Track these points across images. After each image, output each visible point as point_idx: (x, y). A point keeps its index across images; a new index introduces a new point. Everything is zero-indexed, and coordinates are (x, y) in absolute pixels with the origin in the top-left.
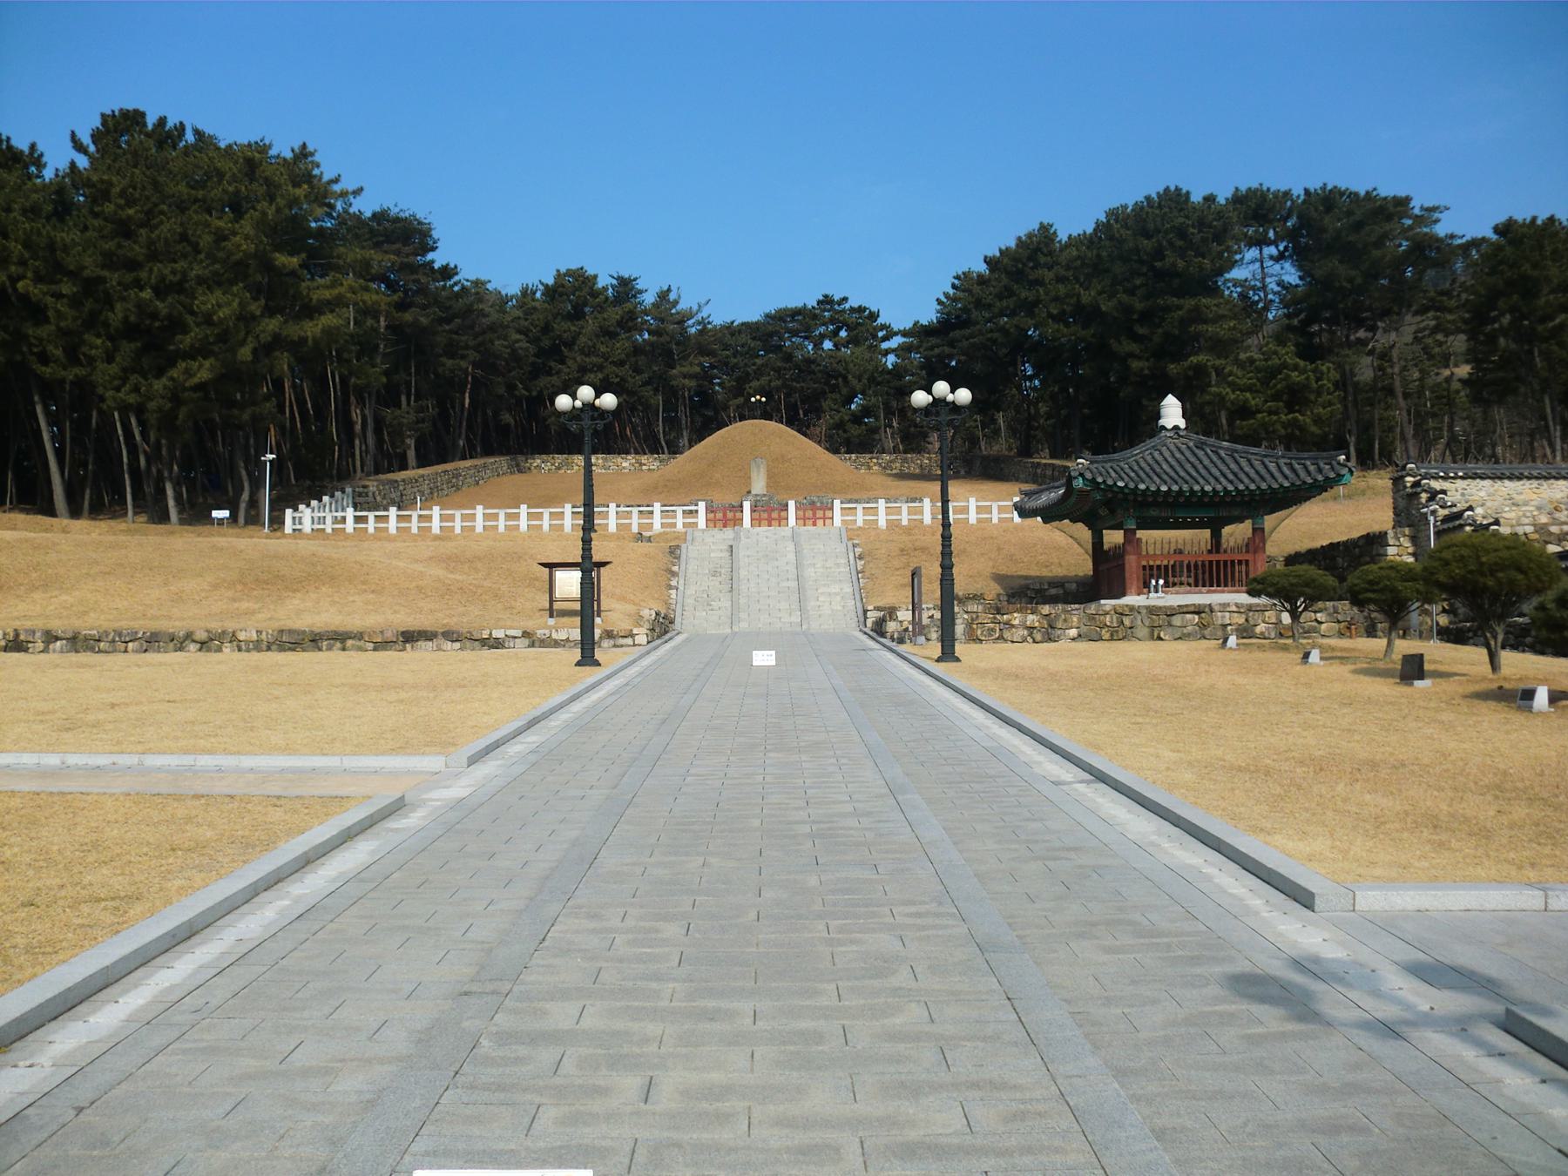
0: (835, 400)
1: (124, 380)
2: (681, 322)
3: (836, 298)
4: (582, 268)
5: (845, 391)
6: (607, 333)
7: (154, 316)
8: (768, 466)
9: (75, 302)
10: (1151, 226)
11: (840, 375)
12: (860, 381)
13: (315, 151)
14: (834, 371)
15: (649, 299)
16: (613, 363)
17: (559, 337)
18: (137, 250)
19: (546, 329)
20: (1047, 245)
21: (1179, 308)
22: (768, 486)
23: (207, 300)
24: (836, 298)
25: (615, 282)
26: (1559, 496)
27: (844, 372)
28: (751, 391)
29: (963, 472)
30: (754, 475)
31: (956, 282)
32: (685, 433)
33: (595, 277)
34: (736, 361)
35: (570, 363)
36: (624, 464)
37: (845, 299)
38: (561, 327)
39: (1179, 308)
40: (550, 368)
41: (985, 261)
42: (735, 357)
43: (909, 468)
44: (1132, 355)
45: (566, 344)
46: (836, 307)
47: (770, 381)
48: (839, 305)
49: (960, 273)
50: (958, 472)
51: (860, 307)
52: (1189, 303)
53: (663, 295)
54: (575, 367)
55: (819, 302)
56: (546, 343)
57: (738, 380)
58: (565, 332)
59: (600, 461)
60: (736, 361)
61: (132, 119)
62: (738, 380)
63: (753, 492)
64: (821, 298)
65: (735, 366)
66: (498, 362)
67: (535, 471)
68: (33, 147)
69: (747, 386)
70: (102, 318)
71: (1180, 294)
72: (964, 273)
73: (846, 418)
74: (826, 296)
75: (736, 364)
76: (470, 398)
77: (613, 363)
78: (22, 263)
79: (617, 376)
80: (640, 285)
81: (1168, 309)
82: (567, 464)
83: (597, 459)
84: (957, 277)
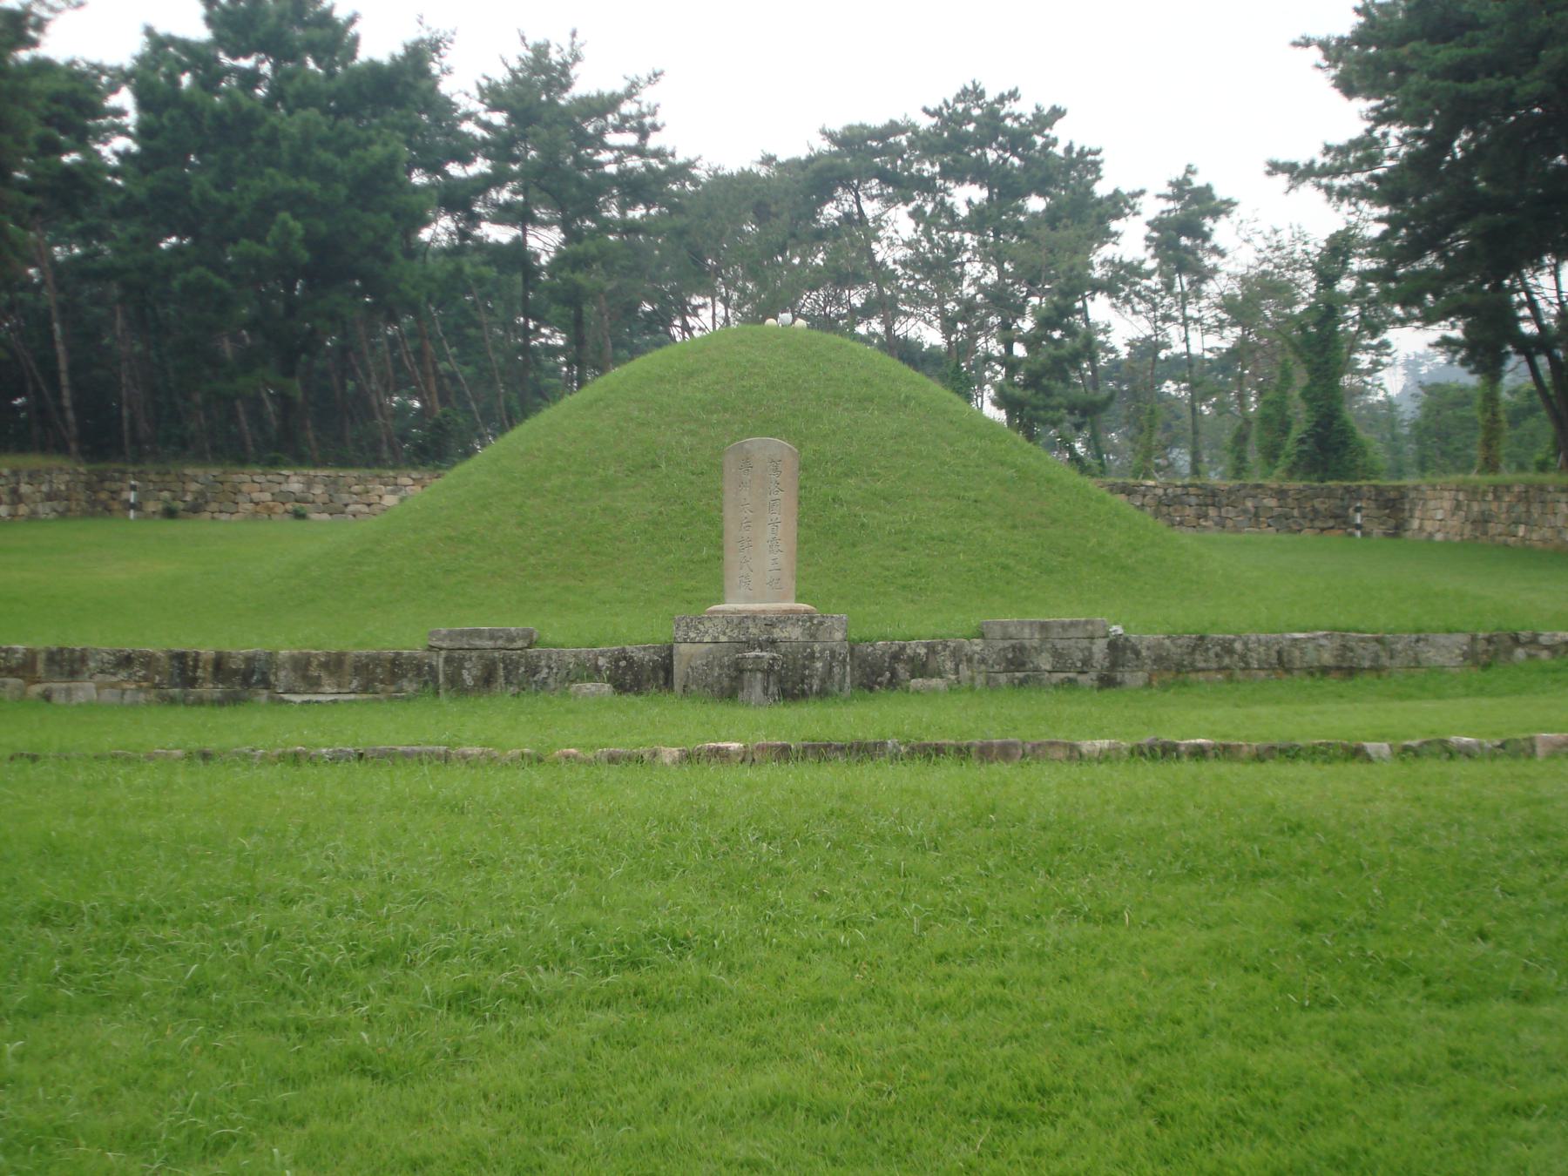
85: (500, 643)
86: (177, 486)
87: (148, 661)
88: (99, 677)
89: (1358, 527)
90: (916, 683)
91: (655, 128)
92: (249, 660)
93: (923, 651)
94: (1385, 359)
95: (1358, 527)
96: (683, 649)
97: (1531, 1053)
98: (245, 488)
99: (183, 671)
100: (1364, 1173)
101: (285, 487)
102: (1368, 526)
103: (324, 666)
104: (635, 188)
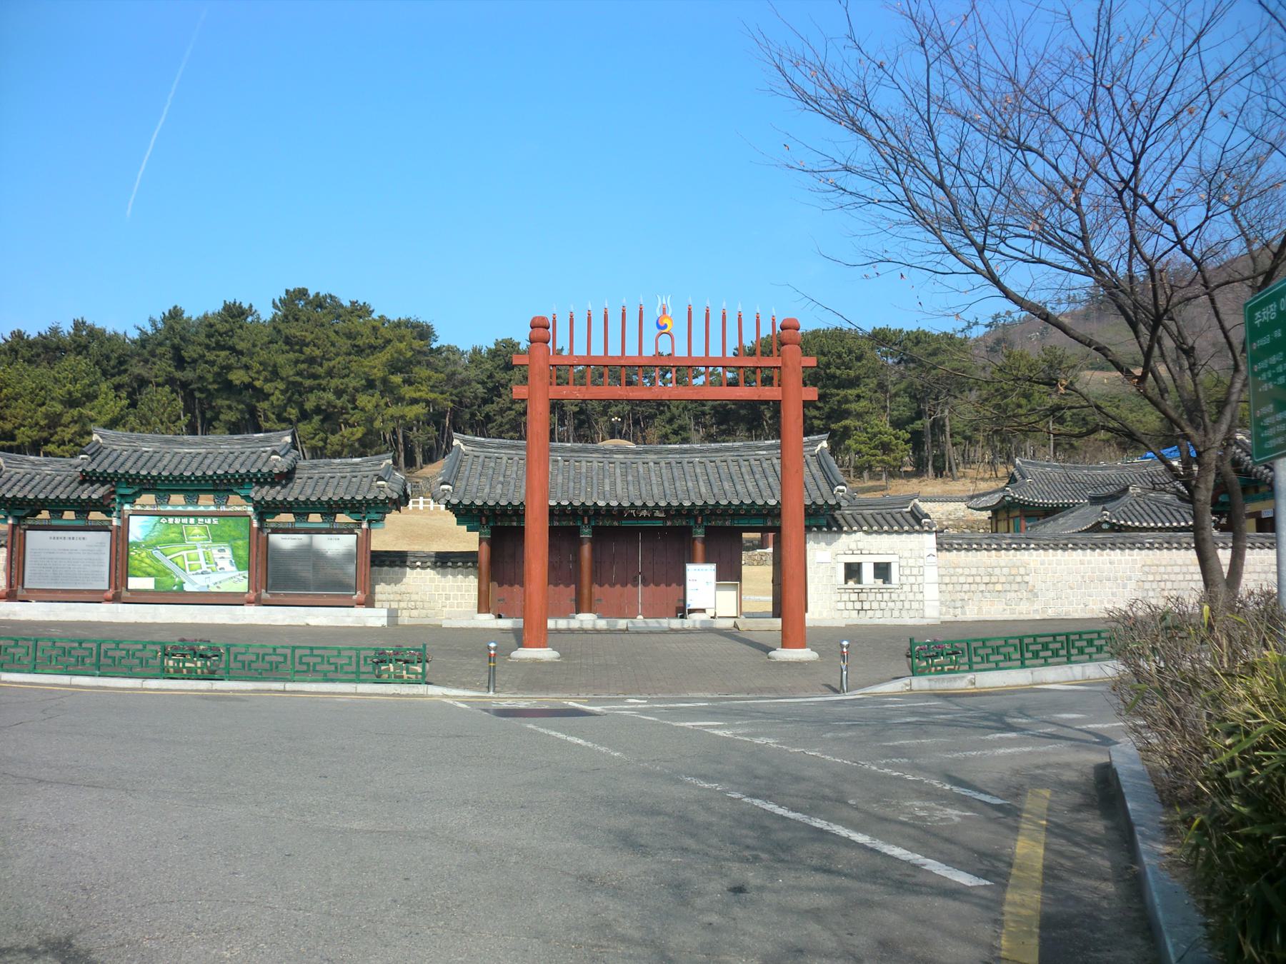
1: (316, 435)
5: (668, 415)
7: (335, 407)
9: (283, 392)
10: (826, 350)
17: (498, 382)
18: (320, 371)
19: (491, 376)
21: (838, 395)
23: (363, 400)
26: (951, 509)
32: (908, 804)
33: (519, 343)
35: (504, 397)
39: (838, 395)
44: (815, 417)
45: (502, 386)
52: (842, 392)
54: (508, 400)
56: (490, 385)
57: (604, 406)
61: (302, 293)
62: (604, 406)
68: (251, 306)
71: (837, 387)
78: (258, 372)
81: (832, 395)
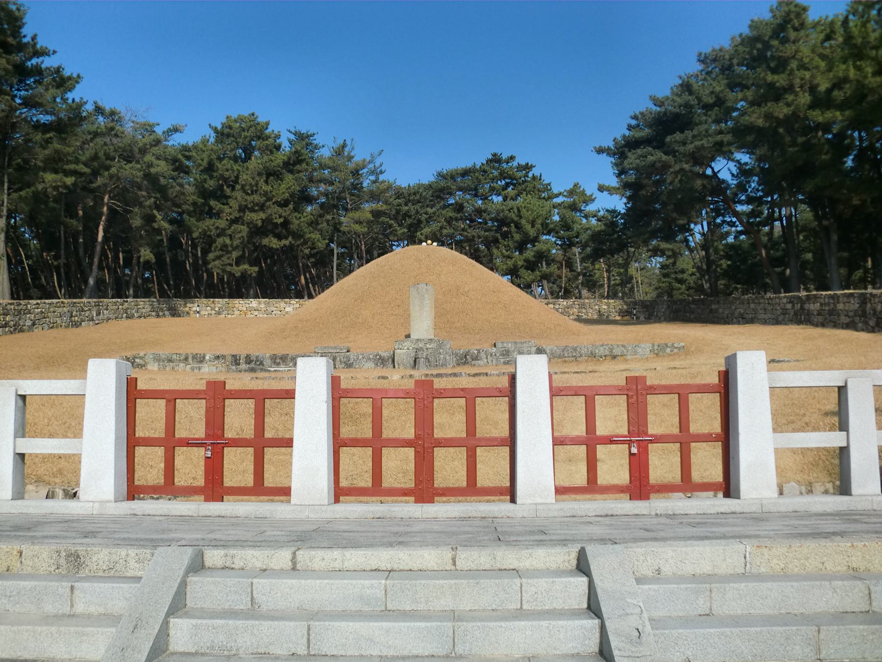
0: (507, 247)
2: (356, 173)
3: (504, 157)
4: (253, 114)
5: (517, 237)
6: (271, 174)
8: (436, 300)
11: (513, 221)
12: (533, 226)
13: (54, 52)
14: (506, 218)
15: (325, 153)
16: (276, 203)
20: (798, 15)
22: (436, 327)
24: (504, 157)
25: (292, 137)
27: (516, 219)
28: (423, 238)
29: (642, 318)
30: (415, 312)
31: (634, 122)
34: (407, 208)
36: (288, 309)
37: (512, 158)
38: (225, 167)
40: (211, 208)
41: (699, 60)
42: (406, 205)
43: (586, 314)
46: (505, 165)
47: (441, 228)
48: (508, 163)
49: (637, 113)
50: (638, 318)
51: (527, 164)
53: (339, 151)
55: (489, 161)
58: (227, 170)
59: (262, 306)
60: (407, 208)
63: (414, 336)
64: (490, 157)
65: (407, 215)
66: (139, 193)
67: (192, 315)
69: (418, 234)
70: (33, 235)
72: (642, 114)
73: (520, 263)
74: (495, 155)
75: (408, 211)
76: (105, 231)
77: (276, 203)
79: (280, 217)
80: (318, 140)
82: (228, 309)
83: (260, 303)
84: (635, 117)
85: (338, 351)
86: (213, 305)
87: (224, 357)
88: (209, 363)
89: (635, 315)
90: (473, 362)
91: (381, 172)
92: (257, 357)
93: (476, 352)
94: (214, 157)
95: (635, 315)
96: (397, 351)
97: (657, 515)
98: (236, 305)
99: (235, 361)
100: (530, 661)
101: (251, 305)
102: (639, 315)
103: (281, 358)
104: (374, 196)
